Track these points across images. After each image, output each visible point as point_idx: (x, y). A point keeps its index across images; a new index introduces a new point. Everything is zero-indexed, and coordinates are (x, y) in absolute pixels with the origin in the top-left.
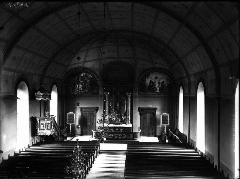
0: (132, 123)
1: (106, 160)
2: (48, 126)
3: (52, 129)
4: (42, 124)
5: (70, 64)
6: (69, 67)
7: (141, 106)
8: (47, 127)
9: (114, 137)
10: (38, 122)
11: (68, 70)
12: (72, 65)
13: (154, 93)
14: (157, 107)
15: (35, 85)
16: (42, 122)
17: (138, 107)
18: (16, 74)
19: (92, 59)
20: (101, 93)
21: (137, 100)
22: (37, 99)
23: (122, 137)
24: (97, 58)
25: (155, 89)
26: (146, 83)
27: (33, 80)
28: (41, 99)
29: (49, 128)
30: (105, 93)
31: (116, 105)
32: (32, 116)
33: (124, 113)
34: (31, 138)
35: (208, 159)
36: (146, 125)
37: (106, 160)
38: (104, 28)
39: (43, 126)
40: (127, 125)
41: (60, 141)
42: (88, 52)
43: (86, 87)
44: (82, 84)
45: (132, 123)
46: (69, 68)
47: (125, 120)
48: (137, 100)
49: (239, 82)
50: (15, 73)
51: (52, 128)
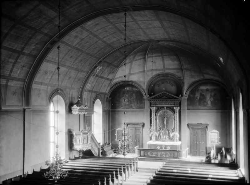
0: (180, 140)
1: (151, 125)
3: (88, 144)
6: (114, 81)
7: (190, 122)
8: (83, 141)
9: (157, 155)
10: (75, 137)
11: (91, 77)
12: (117, 78)
13: (205, 108)
14: (208, 123)
15: (73, 99)
18: (49, 87)
19: (137, 71)
20: (147, 104)
23: (165, 155)
24: (142, 70)
25: (206, 102)
26: (196, 96)
27: (71, 94)
29: (85, 143)
30: (151, 108)
32: (70, 128)
33: (172, 130)
34: (68, 153)
36: (197, 143)
37: (151, 125)
38: (152, 54)
39: (79, 141)
40: (175, 142)
42: (132, 64)
46: (115, 81)
47: (173, 137)
49: (241, 94)
50: (48, 87)
51: (89, 142)
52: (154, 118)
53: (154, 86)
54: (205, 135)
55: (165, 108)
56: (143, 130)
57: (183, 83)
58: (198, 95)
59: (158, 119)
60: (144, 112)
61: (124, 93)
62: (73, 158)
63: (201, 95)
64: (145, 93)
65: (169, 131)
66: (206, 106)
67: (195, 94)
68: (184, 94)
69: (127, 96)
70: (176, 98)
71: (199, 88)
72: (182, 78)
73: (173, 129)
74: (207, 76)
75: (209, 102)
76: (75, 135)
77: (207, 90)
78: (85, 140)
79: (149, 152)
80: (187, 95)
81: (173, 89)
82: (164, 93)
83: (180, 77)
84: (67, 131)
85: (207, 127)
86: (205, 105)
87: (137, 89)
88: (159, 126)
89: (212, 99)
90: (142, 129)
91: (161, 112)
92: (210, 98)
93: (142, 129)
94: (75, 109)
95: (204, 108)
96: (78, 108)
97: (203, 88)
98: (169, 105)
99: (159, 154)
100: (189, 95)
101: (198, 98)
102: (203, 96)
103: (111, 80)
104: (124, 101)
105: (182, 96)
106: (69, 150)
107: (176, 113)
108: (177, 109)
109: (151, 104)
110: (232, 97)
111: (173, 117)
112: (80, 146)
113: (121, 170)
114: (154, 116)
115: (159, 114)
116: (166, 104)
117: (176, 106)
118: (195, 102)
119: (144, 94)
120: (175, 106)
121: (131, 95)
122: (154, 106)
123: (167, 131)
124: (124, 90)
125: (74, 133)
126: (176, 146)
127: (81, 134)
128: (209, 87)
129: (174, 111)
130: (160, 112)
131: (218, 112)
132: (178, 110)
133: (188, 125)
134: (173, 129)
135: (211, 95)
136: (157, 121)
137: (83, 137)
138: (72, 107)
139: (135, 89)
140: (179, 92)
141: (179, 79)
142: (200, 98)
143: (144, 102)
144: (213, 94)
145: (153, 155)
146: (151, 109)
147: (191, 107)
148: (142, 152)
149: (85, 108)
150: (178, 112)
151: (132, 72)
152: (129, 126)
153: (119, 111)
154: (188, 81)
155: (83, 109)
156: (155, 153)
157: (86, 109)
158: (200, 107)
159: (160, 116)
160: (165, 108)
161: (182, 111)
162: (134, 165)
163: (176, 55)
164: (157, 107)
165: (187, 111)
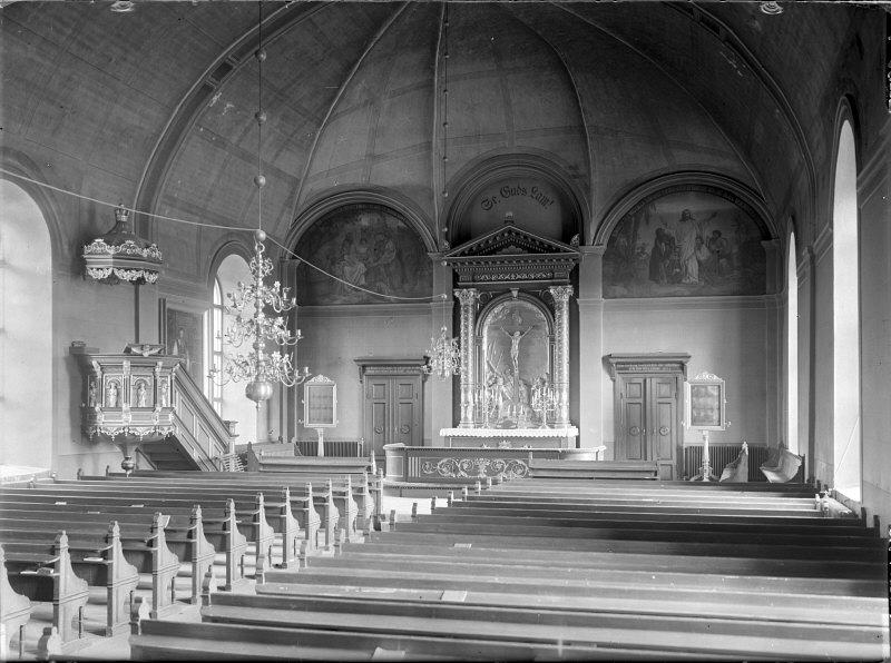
0: (574, 422)
2: (138, 395)
4: (113, 385)
5: (312, 174)
6: (309, 187)
13: (677, 288)
14: (690, 353)
16: (110, 377)
17: (603, 353)
21: (601, 318)
22: (90, 273)
26: (639, 243)
28: (110, 271)
30: (457, 294)
31: (507, 346)
34: (69, 448)
35: (870, 524)
39: (118, 394)
41: (232, 473)
43: (382, 270)
44: (365, 260)
45: (574, 422)
48: (601, 318)
49: (847, 131)
52: (471, 335)
53: (471, 206)
54: (673, 400)
55: (515, 293)
56: (426, 384)
57: (588, 188)
58: (646, 240)
59: (485, 340)
60: (429, 312)
61: (349, 240)
62: (104, 475)
63: (660, 236)
64: (433, 233)
65: (528, 386)
66: (680, 282)
67: (635, 236)
68: (593, 232)
69: (363, 250)
70: (558, 250)
71: (652, 211)
72: (582, 171)
73: (545, 377)
74: (684, 159)
75: (693, 267)
76: (98, 370)
77: (685, 217)
78: (143, 392)
79: (445, 460)
80: (604, 239)
81: (544, 217)
82: (510, 232)
83: (575, 168)
84: (63, 353)
85: (682, 366)
86: (676, 280)
87: (401, 224)
88: (492, 369)
89: (704, 254)
90: (423, 382)
91: (498, 310)
92: (698, 248)
93: (423, 382)
94: (102, 258)
95: (672, 290)
96: (112, 251)
97: (670, 208)
98: (531, 278)
99: (482, 469)
100: (612, 241)
101: (649, 250)
102: (670, 241)
103: (295, 182)
104: (351, 274)
105: (582, 243)
106: (72, 435)
107: (557, 313)
108: (562, 296)
109: (456, 277)
110: (790, 224)
111: (547, 329)
112: (120, 417)
113: (281, 505)
114: (471, 328)
115: (489, 319)
116: (519, 276)
117: (559, 284)
118: (639, 269)
119: (429, 241)
120: (553, 284)
121: (378, 250)
122: (467, 287)
123: (523, 388)
124: (348, 227)
125: (94, 363)
126: (559, 440)
127: (126, 364)
128: (695, 205)
129: (550, 307)
130: (496, 310)
131: (724, 305)
132: (566, 299)
133: (607, 360)
134: (545, 377)
135: (699, 237)
136: (480, 348)
137: (133, 380)
138: (87, 249)
139: (394, 223)
140: (572, 227)
141: (570, 172)
142: (656, 248)
143: (431, 274)
144: (707, 233)
145: (456, 470)
146: (456, 300)
147: (619, 289)
148: (414, 461)
149: (145, 253)
150: (565, 308)
151: (378, 151)
152: (369, 371)
153: (329, 314)
154: (607, 174)
155: (138, 257)
156: (465, 466)
157: (150, 259)
158: (655, 288)
159: (494, 328)
160: (515, 293)
161: (580, 305)
162: (359, 498)
163: (560, 67)
164: (479, 289)
165: (602, 304)
